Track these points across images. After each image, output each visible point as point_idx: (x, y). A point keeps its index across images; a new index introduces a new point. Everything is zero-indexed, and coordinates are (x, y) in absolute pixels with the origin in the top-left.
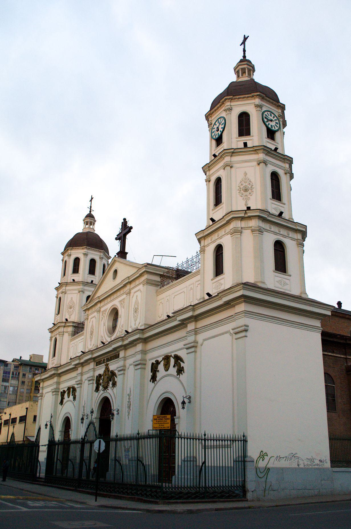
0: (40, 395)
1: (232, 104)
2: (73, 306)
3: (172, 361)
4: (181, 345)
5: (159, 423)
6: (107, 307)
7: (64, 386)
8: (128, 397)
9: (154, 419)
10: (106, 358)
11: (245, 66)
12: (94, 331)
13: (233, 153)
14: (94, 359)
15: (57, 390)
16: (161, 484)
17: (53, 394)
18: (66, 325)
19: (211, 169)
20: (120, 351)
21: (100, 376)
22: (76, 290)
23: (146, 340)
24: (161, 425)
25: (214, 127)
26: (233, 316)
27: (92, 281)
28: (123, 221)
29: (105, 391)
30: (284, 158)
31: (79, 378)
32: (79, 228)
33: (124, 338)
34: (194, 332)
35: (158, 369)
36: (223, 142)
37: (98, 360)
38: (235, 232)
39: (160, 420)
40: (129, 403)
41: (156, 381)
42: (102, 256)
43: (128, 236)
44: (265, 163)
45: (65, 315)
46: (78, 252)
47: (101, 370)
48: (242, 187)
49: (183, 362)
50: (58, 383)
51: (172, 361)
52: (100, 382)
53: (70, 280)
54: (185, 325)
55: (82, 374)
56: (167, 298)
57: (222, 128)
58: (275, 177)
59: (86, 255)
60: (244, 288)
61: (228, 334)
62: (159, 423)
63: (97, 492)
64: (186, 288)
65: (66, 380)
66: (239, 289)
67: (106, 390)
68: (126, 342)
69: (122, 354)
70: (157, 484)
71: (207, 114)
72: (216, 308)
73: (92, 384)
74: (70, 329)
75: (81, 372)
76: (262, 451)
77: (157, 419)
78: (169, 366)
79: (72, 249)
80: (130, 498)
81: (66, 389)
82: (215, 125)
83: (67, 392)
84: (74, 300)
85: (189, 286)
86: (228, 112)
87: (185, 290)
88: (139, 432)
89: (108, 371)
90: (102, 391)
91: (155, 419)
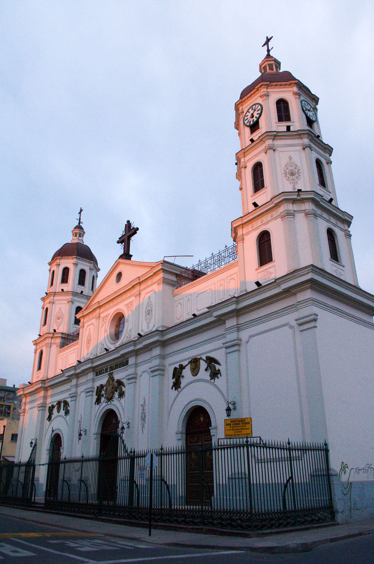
0: (22, 411)
1: (269, 90)
3: (203, 365)
4: (219, 343)
5: (235, 430)
6: (110, 312)
7: (51, 401)
8: (141, 408)
9: (227, 424)
10: (109, 367)
11: (77, 231)
12: (92, 339)
13: (275, 136)
14: (93, 369)
15: (44, 405)
16: (200, 507)
17: (87, 395)
18: (54, 336)
19: (247, 155)
20: (227, 319)
21: (102, 386)
22: (65, 300)
23: (164, 344)
24: (238, 432)
25: (247, 115)
26: (294, 304)
27: (82, 292)
28: (126, 223)
29: (109, 403)
30: (324, 147)
31: (73, 390)
32: (69, 239)
33: (136, 342)
34: (236, 328)
35: (182, 374)
36: (260, 128)
37: (98, 371)
38: (288, 214)
39: (235, 426)
40: (143, 415)
41: (180, 387)
42: (92, 268)
43: (133, 238)
44: (311, 149)
45: (53, 325)
46: (68, 262)
47: (103, 380)
48: (287, 171)
49: (219, 364)
50: (45, 397)
51: (203, 365)
52: (102, 393)
53: (59, 289)
54: (223, 321)
55: (77, 386)
57: (258, 114)
58: (318, 163)
59: (76, 264)
60: (313, 271)
61: (287, 328)
62: (235, 430)
63: (150, 523)
64: (77, 349)
65: (187, 348)
66: (307, 272)
67: (111, 402)
68: (139, 346)
69: (132, 361)
70: (183, 507)
71: (238, 103)
72: (279, 294)
73: (91, 396)
74: (59, 341)
75: (75, 383)
76: (343, 462)
77: (230, 424)
78: (198, 370)
79: (60, 258)
80: (192, 528)
81: (55, 404)
82: (248, 113)
83: (56, 407)
84: (63, 310)
85: (218, 282)
86: (265, 98)
87: (235, 276)
88: (163, 447)
89: (113, 380)
90: (104, 403)
91: (227, 425)
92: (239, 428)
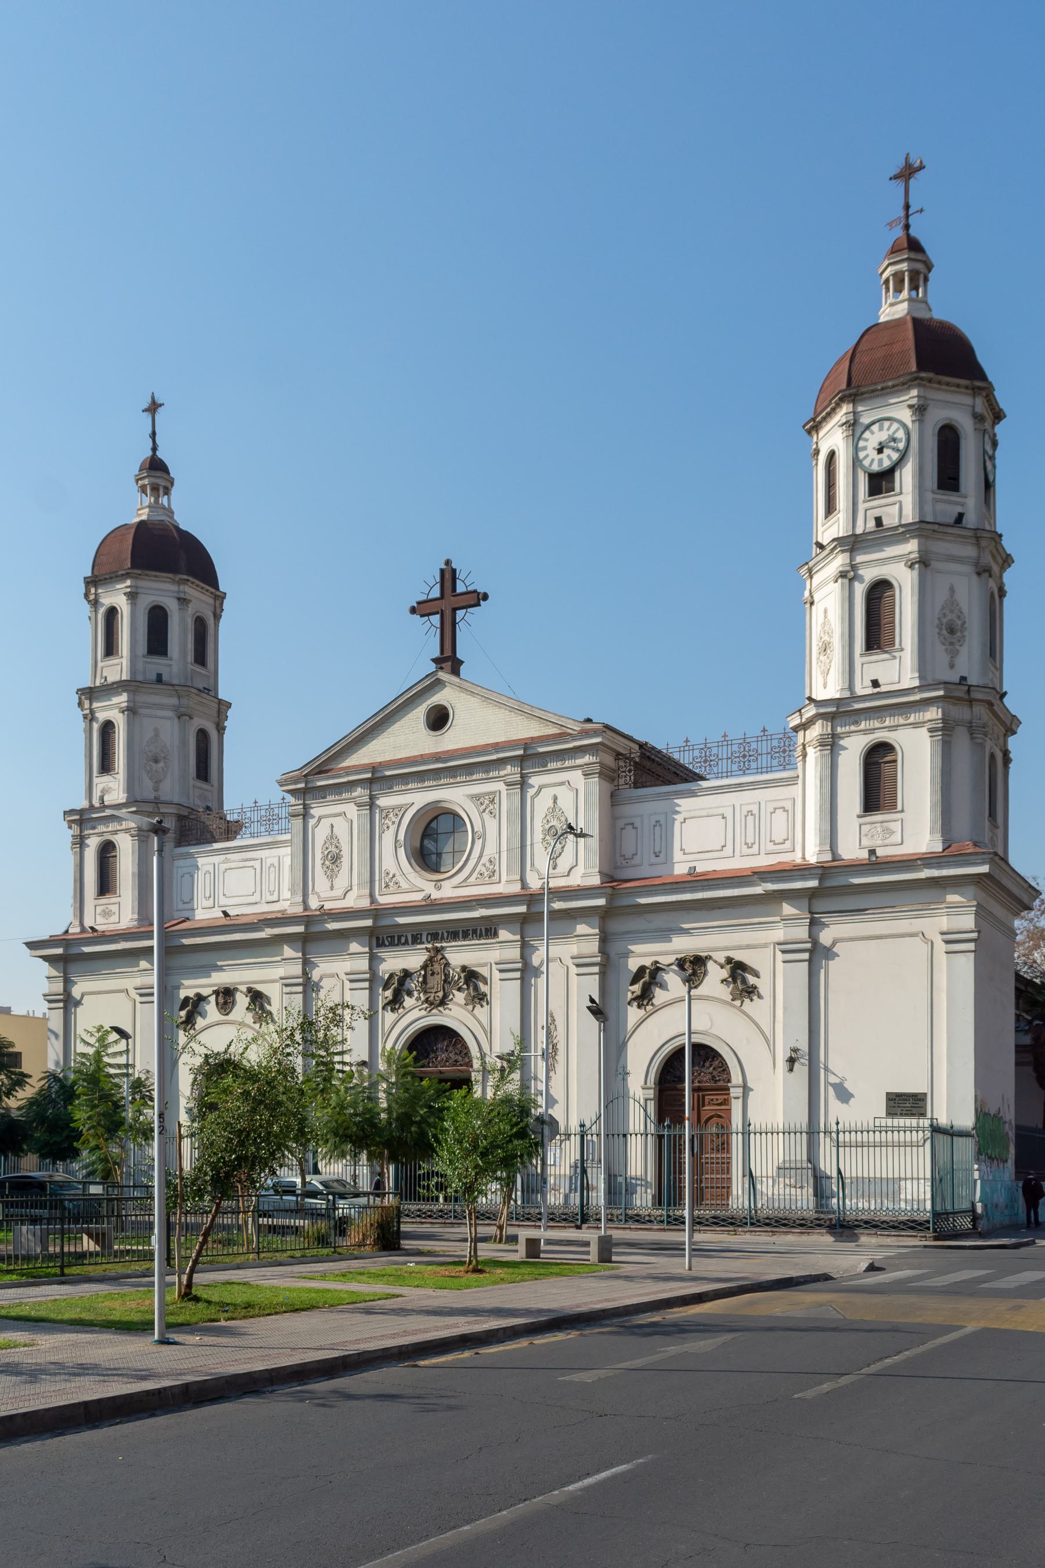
2: (163, 755)
49: (756, 975)
56: (657, 817)
59: (183, 601)
61: (918, 940)
92: (908, 1105)
